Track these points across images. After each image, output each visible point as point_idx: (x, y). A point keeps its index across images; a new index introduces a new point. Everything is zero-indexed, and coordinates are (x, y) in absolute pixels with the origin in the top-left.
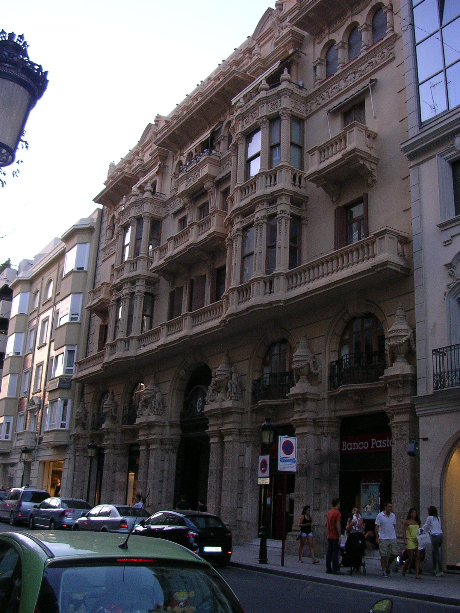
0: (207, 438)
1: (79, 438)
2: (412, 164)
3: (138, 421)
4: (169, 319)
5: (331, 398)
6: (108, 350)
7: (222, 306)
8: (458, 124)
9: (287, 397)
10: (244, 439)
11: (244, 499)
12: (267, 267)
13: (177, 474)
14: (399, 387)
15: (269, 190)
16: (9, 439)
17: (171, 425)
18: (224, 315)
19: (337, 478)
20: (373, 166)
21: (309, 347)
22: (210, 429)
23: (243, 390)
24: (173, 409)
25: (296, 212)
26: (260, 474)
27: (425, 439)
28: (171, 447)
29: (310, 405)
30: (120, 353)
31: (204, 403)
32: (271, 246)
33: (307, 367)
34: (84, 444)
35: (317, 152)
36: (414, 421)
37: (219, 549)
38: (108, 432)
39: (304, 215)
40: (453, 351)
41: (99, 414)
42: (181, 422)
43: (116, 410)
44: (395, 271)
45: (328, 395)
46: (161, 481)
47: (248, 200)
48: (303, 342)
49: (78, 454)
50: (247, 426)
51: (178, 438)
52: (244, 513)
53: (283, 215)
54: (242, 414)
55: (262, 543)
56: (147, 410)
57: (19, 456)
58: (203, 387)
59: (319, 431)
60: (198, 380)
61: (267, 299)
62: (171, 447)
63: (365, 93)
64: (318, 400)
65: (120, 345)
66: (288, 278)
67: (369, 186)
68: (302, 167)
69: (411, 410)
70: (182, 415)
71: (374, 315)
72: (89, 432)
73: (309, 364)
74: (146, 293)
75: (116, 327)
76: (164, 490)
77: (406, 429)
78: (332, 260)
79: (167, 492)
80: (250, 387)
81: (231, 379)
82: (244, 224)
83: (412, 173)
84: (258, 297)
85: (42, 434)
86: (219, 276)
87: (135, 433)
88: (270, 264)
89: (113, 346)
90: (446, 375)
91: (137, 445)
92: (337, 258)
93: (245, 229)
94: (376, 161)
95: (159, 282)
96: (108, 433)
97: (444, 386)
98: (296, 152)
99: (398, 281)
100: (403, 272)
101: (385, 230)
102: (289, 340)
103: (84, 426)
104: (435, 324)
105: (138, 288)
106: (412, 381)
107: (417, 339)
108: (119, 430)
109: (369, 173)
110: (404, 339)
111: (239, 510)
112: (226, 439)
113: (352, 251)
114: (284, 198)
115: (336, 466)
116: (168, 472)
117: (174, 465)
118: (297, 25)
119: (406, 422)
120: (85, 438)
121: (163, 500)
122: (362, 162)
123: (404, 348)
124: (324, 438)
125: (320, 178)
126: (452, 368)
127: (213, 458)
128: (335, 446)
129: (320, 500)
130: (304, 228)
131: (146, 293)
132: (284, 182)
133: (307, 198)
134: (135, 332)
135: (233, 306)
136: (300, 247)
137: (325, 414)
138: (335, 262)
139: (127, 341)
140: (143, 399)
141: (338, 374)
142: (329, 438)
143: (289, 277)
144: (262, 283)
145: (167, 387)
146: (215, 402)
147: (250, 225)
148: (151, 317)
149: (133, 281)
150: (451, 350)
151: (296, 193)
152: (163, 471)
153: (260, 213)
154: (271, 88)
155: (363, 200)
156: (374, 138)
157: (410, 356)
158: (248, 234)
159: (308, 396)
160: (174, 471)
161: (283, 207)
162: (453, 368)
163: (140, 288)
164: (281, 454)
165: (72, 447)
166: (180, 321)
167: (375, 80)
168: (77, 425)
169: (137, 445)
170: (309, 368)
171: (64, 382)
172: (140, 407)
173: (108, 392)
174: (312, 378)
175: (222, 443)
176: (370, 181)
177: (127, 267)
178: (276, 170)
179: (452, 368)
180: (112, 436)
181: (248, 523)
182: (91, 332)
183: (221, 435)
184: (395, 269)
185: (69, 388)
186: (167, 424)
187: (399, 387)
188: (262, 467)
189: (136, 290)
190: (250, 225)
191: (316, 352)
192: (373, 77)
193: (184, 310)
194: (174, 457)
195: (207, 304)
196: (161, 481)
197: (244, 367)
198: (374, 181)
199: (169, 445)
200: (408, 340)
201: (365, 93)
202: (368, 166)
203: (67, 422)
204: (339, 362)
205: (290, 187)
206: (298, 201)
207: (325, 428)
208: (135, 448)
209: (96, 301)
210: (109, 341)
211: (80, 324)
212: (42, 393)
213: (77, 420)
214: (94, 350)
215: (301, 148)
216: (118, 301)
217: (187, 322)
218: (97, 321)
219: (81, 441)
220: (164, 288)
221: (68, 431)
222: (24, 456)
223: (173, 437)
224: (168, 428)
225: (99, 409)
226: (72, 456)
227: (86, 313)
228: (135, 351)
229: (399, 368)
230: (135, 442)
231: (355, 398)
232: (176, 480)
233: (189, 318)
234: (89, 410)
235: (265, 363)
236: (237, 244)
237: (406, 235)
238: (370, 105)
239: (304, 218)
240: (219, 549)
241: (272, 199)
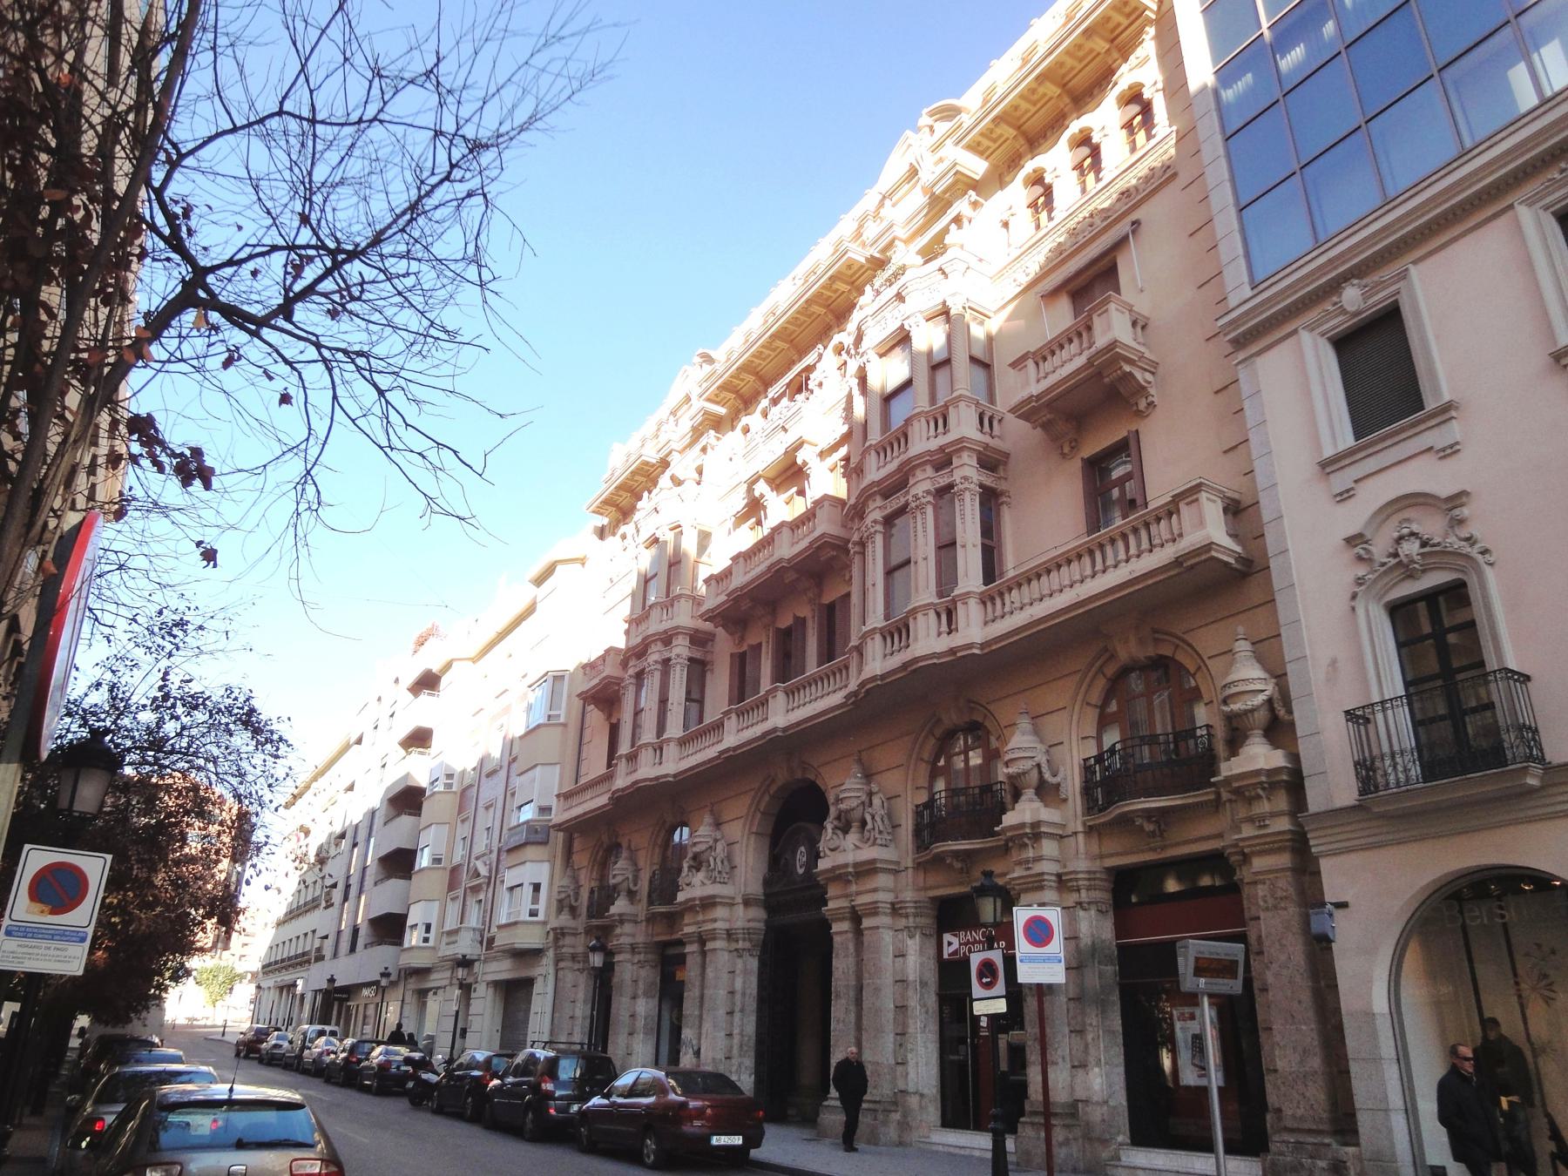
0: (826, 925)
1: (563, 934)
2: (1241, 356)
3: (681, 897)
4: (1089, 533)
5: (918, 866)
6: (622, 766)
7: (847, 668)
8: (1562, 130)
9: (997, 834)
10: (902, 922)
11: (910, 1046)
12: (939, 583)
13: (762, 1000)
14: (1026, 845)
15: (934, 444)
16: (431, 943)
17: (747, 902)
18: (853, 686)
19: (1115, 997)
20: (1149, 377)
21: (1036, 732)
22: (831, 905)
23: (895, 826)
24: (750, 867)
25: (988, 482)
26: (977, 991)
27: (1342, 905)
28: (747, 945)
29: (1048, 847)
30: (647, 770)
31: (815, 856)
32: (947, 547)
33: (1035, 771)
34: (633, 936)
35: (1030, 363)
36: (1306, 868)
37: (737, 1140)
38: (622, 919)
39: (1002, 486)
40: (1390, 712)
41: (601, 888)
42: (765, 894)
43: (577, 894)
44: (1226, 564)
45: (1084, 824)
46: (731, 1013)
47: (892, 466)
48: (1024, 723)
49: (561, 965)
50: (909, 895)
51: (761, 925)
52: (912, 1075)
53: (966, 485)
54: (896, 872)
55: (995, 1142)
56: (701, 875)
57: (448, 974)
58: (810, 826)
59: (1072, 898)
60: (797, 814)
61: (942, 644)
62: (747, 945)
63: (1122, 243)
64: (1062, 837)
65: (646, 756)
66: (984, 603)
67: (1140, 414)
68: (992, 400)
69: (1299, 845)
70: (767, 883)
71: (1172, 659)
72: (580, 923)
73: (1039, 766)
74: (690, 659)
75: (636, 726)
76: (736, 1031)
77: (1285, 884)
78: (1079, 557)
79: (742, 1035)
80: (910, 822)
81: (871, 804)
82: (889, 510)
83: (1243, 374)
84: (928, 641)
85: (494, 929)
86: (833, 619)
87: (672, 919)
88: (947, 575)
89: (632, 758)
90: (1388, 762)
91: (681, 943)
92: (1091, 553)
93: (889, 521)
94: (1153, 368)
95: (1005, 463)
96: (622, 922)
97: (1377, 789)
98: (980, 374)
99: (1232, 583)
100: (1238, 566)
101: (1200, 485)
102: (987, 724)
103: (573, 911)
104: (1334, 662)
105: (676, 651)
106: (1293, 783)
107: (1293, 695)
108: (642, 917)
109: (1141, 390)
110: (1261, 698)
111: (900, 1068)
112: (866, 923)
113: (1113, 541)
114: (965, 455)
115: (1111, 970)
116: (744, 994)
117: (754, 980)
118: (708, 400)
119: (1283, 870)
120: (575, 935)
121: (735, 1051)
122: (1127, 368)
123: (1262, 716)
124: (1082, 913)
125: (1028, 411)
126: (1370, 751)
127: (842, 966)
128: (1106, 930)
129: (1086, 1046)
130: (1005, 509)
131: (690, 659)
132: (964, 425)
133: (1007, 455)
134: (674, 729)
135: (878, 662)
136: (1000, 546)
137: (1082, 865)
138: (1087, 560)
139: (659, 749)
140: (690, 855)
141: (1105, 785)
142: (1093, 912)
143: (986, 600)
144: (932, 614)
145: (735, 830)
146: (840, 851)
147: (902, 511)
148: (701, 702)
149: (667, 639)
150: (1384, 710)
151: (987, 446)
152: (732, 993)
153: (654, 656)
154: (926, 262)
155: (1125, 448)
156: (1143, 328)
157: (1279, 728)
158: (894, 531)
159: (1043, 829)
160: (755, 992)
161: (967, 471)
162: (1396, 748)
163: (681, 649)
164: (1022, 946)
165: (551, 953)
166: (764, 702)
167: (1136, 224)
168: (560, 910)
169: (681, 943)
170: (1040, 772)
171: (536, 832)
172: (685, 869)
173: (619, 846)
174: (1047, 792)
175: (858, 932)
176: (1142, 405)
177: (655, 614)
178: (946, 406)
179: (1370, 751)
180: (628, 928)
181: (922, 1095)
182: (586, 740)
183: (856, 917)
184: (1225, 558)
185: (545, 843)
186: (739, 900)
187: (1259, 797)
188: (981, 975)
189: (673, 655)
190: (902, 511)
191: (1049, 742)
192: (1134, 216)
193: (766, 684)
194: (754, 964)
195: (812, 669)
196: (731, 1013)
197: (892, 781)
198: (1151, 405)
199: (1089, 889)
200: (1270, 701)
201: (1122, 243)
202: (1138, 375)
203: (541, 907)
204: (930, 804)
205: (977, 436)
206: (991, 461)
207: (1084, 893)
208: (672, 951)
209: (596, 681)
210: (624, 748)
211: (564, 725)
212: (494, 856)
213: (560, 901)
214: (595, 765)
215: (987, 366)
216: (640, 676)
217: (779, 702)
218: (595, 716)
219: (568, 940)
220: (724, 647)
221: (544, 923)
222: (460, 973)
223: (752, 924)
224: (741, 907)
225: (603, 877)
226: (551, 970)
227: (578, 703)
228: (673, 763)
229: (1259, 756)
230: (675, 937)
231: (958, 865)
232: (759, 1010)
233: (781, 696)
234: (582, 882)
235: (934, 774)
236: (877, 548)
237: (1236, 496)
238: (1130, 269)
239: (1002, 493)
240: (737, 1140)
241: (943, 460)
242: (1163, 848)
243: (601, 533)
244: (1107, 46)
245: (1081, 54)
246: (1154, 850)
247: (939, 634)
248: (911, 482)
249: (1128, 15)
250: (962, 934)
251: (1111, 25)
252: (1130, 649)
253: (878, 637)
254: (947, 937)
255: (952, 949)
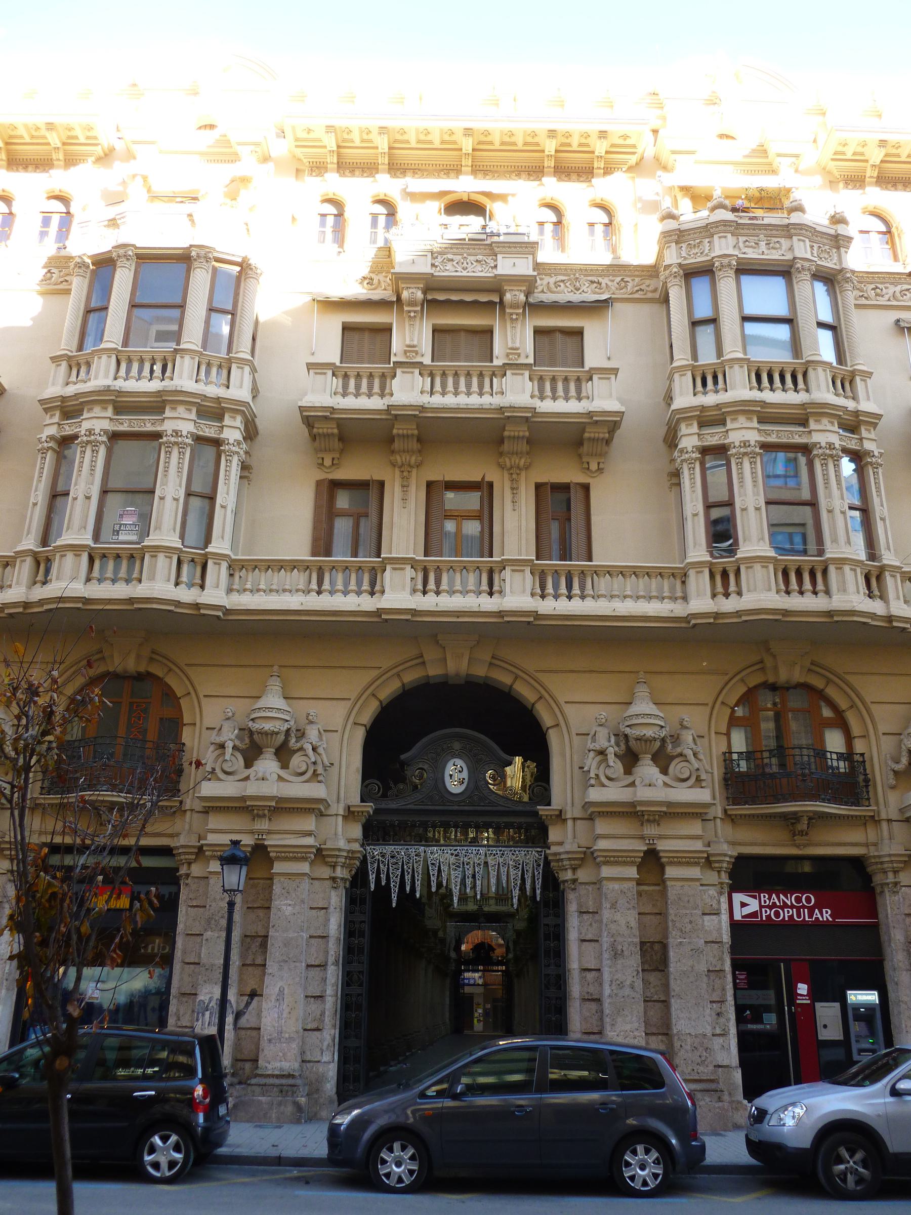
187: (264, 816)
242: (805, 846)
243: (513, 195)
244: (59, 145)
245: (34, 133)
246: (798, 846)
247: (88, 580)
248: (86, 415)
249: (32, 137)
250: (764, 897)
251: (72, 133)
252: (789, 672)
253: (29, 560)
254: (738, 898)
255: (747, 911)
